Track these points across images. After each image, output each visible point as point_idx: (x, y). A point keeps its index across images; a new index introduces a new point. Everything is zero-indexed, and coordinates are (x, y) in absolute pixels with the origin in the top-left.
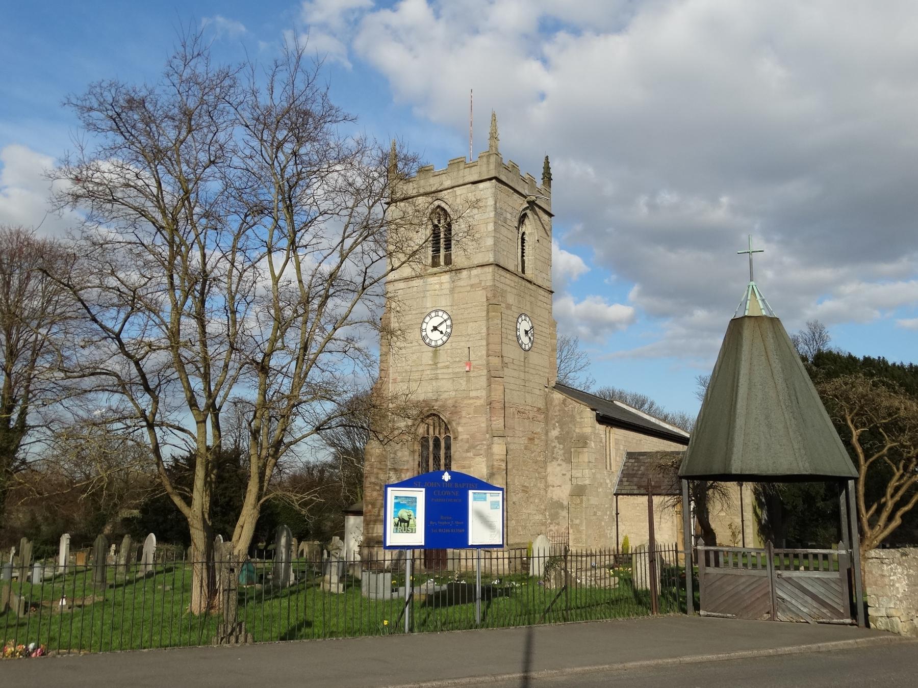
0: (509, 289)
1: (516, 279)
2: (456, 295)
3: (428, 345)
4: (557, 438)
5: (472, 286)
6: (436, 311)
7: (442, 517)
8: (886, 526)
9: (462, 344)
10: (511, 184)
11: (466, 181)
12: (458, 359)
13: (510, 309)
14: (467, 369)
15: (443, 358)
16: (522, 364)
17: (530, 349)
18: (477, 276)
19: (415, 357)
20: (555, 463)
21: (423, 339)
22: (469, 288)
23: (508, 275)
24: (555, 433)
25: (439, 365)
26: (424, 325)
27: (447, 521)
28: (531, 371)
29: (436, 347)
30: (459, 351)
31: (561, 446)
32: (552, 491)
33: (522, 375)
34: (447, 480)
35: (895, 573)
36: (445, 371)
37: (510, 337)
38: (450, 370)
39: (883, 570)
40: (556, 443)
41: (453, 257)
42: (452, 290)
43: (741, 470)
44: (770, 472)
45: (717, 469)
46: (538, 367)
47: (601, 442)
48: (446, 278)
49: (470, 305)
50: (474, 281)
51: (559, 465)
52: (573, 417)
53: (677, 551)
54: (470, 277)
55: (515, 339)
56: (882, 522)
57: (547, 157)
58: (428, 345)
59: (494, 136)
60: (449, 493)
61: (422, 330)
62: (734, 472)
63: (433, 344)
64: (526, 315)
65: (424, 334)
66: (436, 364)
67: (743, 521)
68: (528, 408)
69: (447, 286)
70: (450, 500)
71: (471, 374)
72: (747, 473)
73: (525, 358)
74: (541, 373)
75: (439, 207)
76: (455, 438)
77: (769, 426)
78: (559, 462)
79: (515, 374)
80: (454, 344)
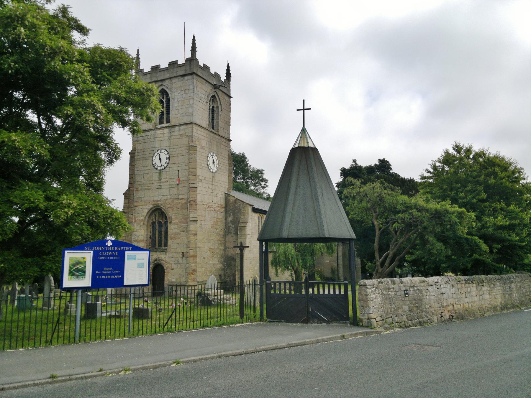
0: (203, 138)
1: (208, 132)
2: (172, 140)
3: (156, 169)
4: (231, 221)
5: (181, 135)
6: (161, 149)
7: (105, 269)
8: (390, 265)
9: (175, 169)
10: (204, 78)
11: (178, 75)
12: (172, 177)
13: (204, 149)
14: (178, 183)
15: (164, 175)
16: (211, 180)
17: (216, 172)
18: (184, 129)
19: (148, 176)
20: (230, 235)
21: (153, 165)
22: (179, 137)
23: (203, 130)
24: (230, 219)
25: (162, 180)
26: (154, 157)
27: (108, 271)
28: (216, 184)
29: (160, 170)
30: (173, 173)
31: (233, 226)
32: (228, 251)
33: (211, 187)
34: (109, 245)
35: (374, 294)
36: (165, 184)
37: (203, 165)
38: (168, 183)
39: (367, 292)
40: (230, 224)
41: (170, 118)
42: (170, 138)
43: (288, 235)
44: (304, 236)
45: (275, 236)
46: (221, 182)
47: (256, 223)
48: (166, 131)
49: (179, 146)
50: (182, 132)
51: (232, 236)
52: (240, 210)
53: (255, 285)
54: (179, 130)
55: (207, 166)
56: (386, 264)
57: (228, 64)
58: (156, 169)
59: (194, 49)
60: (110, 253)
61: (152, 160)
62: (283, 237)
63: (159, 168)
64: (213, 153)
65: (154, 162)
66: (160, 180)
67: (338, 265)
68: (214, 205)
69: (167, 135)
70: (112, 258)
71: (180, 186)
72: (291, 237)
73: (213, 177)
74: (223, 185)
75: (163, 89)
76: (170, 222)
77: (305, 210)
78: (232, 235)
79: (207, 185)
80: (171, 169)
